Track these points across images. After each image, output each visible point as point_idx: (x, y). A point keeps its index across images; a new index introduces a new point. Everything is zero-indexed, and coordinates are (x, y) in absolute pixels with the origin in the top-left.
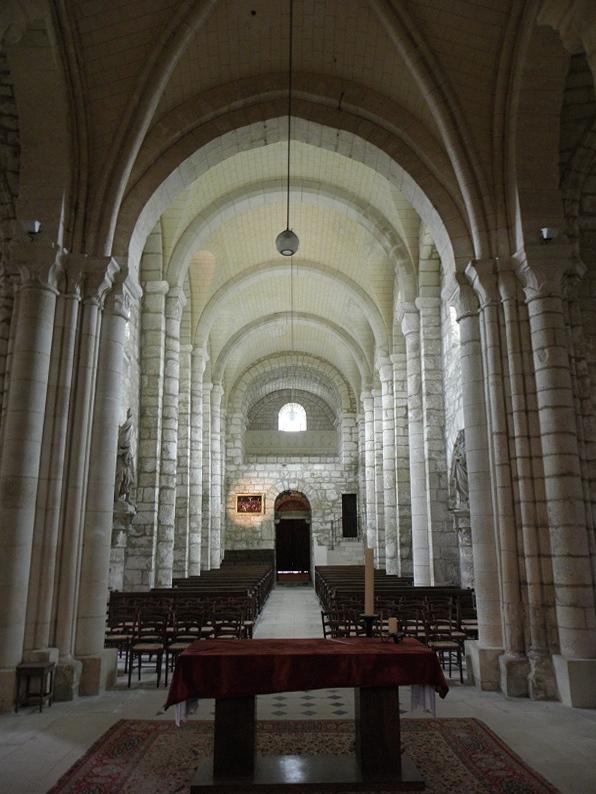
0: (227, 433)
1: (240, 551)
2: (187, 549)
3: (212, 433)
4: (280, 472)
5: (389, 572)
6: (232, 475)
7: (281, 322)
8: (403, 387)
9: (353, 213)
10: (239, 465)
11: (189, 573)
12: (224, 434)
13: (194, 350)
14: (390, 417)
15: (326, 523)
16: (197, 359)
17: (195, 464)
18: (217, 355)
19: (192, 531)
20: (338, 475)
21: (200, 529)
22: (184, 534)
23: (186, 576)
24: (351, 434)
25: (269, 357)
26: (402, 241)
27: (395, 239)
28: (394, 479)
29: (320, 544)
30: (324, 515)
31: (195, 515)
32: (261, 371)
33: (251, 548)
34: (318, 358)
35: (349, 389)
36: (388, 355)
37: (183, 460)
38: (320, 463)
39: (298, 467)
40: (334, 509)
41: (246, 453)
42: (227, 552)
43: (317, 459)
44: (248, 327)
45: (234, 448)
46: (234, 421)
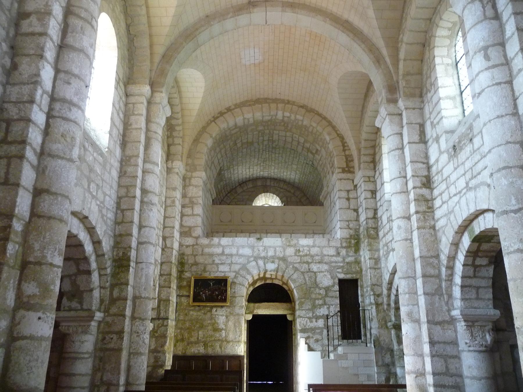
3: (145, 162)
4: (252, 247)
6: (188, 251)
10: (197, 238)
15: (317, 318)
20: (332, 252)
24: (348, 199)
30: (314, 307)
34: (302, 107)
40: (327, 299)
45: (193, 215)
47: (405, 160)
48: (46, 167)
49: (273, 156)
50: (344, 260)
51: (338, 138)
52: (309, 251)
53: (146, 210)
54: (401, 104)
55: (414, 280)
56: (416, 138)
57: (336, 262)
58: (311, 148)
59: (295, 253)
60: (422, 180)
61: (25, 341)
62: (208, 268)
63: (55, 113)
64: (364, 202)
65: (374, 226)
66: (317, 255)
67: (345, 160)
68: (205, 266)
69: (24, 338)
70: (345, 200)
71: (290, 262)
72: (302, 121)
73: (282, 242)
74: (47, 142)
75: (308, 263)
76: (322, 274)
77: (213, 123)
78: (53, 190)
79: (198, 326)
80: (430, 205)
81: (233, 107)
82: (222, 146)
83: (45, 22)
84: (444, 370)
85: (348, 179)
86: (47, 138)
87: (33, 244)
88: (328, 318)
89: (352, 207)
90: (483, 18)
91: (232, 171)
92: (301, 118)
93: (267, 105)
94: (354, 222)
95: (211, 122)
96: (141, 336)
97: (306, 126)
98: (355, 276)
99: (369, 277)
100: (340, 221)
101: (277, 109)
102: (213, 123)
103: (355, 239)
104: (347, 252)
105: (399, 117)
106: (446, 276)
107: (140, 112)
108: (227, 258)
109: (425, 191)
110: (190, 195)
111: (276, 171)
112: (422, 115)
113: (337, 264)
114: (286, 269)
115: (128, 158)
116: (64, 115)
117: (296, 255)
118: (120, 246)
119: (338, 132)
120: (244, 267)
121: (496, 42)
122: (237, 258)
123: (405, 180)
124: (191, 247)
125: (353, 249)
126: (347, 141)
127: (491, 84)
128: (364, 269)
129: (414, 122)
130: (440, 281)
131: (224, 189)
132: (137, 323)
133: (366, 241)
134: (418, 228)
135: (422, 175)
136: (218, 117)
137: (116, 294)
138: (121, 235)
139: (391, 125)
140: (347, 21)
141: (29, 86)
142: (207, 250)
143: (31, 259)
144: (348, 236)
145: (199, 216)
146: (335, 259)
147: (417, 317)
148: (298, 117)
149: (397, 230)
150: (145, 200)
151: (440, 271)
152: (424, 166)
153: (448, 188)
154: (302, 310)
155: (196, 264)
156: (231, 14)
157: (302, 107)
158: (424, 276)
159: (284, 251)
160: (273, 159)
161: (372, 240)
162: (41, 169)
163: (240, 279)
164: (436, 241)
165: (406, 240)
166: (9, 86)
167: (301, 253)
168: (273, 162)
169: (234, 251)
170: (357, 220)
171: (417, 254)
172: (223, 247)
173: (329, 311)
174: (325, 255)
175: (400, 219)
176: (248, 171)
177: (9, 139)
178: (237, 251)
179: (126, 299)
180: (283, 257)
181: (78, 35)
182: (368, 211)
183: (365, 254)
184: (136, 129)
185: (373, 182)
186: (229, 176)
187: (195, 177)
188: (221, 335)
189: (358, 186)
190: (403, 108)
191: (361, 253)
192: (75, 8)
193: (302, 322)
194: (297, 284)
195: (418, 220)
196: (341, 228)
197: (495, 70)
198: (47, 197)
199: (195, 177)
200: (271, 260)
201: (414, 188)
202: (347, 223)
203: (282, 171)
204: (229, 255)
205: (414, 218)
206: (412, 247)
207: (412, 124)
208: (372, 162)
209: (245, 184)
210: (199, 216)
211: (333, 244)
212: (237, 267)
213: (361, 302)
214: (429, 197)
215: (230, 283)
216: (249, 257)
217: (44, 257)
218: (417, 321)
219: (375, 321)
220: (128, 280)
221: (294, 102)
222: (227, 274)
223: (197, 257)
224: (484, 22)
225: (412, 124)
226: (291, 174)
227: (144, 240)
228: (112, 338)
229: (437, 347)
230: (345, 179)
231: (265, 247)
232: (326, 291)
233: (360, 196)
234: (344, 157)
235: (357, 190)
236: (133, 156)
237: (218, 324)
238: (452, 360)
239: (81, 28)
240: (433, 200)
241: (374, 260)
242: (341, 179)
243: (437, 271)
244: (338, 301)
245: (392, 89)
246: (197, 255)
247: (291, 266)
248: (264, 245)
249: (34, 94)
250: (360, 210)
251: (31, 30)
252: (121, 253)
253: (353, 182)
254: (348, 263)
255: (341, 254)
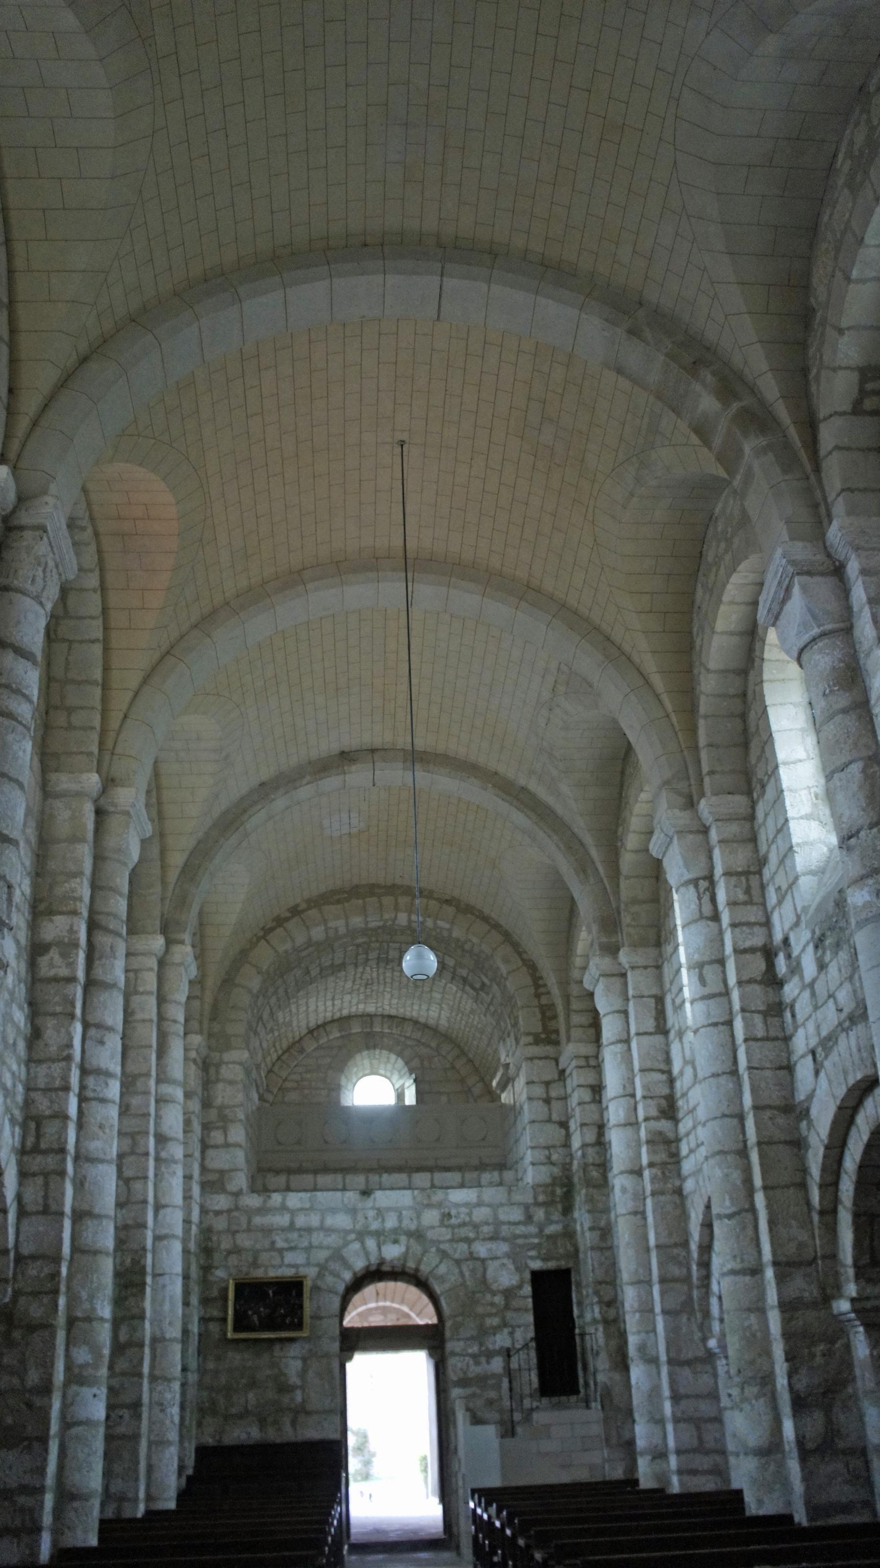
0: (206, 1104)
1: (239, 1449)
2: (54, 1447)
3: (158, 1081)
4: (353, 1211)
5: (755, 1505)
6: (220, 1224)
7: (358, 776)
8: (748, 891)
9: (593, 334)
10: (237, 1194)
11: (56, 1533)
12: (195, 1105)
13: (104, 790)
14: (715, 987)
15: (490, 1355)
16: (114, 823)
17: (94, 1146)
18: (177, 859)
19: (76, 1377)
20: (517, 1215)
21: (104, 1371)
22: (46, 1389)
23: (140, 1514)
24: (547, 1101)
25: (319, 901)
26: (753, 390)
27: (731, 385)
28: (748, 1180)
29: (476, 1421)
30: (484, 1332)
31: (89, 1319)
32: (300, 940)
33: (272, 1435)
34: (448, 902)
35: (537, 981)
36: (690, 804)
37: (50, 1129)
38: (462, 1186)
39: (405, 1198)
40: (509, 1315)
41: (260, 1170)
42: (202, 1452)
43: (456, 1177)
44: (265, 790)
45: (227, 1145)
46: (225, 1072)
47: (632, 1063)
48: (85, 1177)
49: (388, 974)
50: (541, 1231)
51: (525, 969)
52: (470, 1214)
53: (166, 1175)
54: (624, 957)
55: (648, 1287)
56: (650, 1024)
57: (525, 1236)
58: (470, 978)
59: (442, 1221)
60: (659, 1105)
61: (80, 1428)
62: (264, 1257)
63: (90, 1094)
64: (577, 1110)
65: (597, 1161)
66: (487, 1223)
67: (539, 1016)
68: (256, 1254)
69: (79, 1423)
70: (541, 1103)
71: (433, 1242)
72: (450, 931)
73: (414, 1198)
74: (82, 1139)
75: (468, 1241)
76: (497, 1263)
77: (263, 942)
78: (96, 1211)
79: (244, 1381)
80: (673, 1150)
81: (303, 906)
82: (280, 981)
83: (71, 960)
84: (695, 1443)
85: (546, 1058)
86: (82, 1133)
87: (79, 1292)
88: (509, 1356)
89: (555, 1117)
90: (697, 916)
91: (294, 1010)
92: (447, 926)
93: (375, 899)
94: (560, 1150)
95: (259, 939)
96: (169, 1410)
97: (458, 940)
98: (563, 1263)
99: (591, 1268)
100: (532, 1148)
101: (397, 908)
102: (263, 942)
103: (563, 1186)
104: (547, 1213)
105: (622, 980)
106: (698, 1279)
107: (148, 988)
108: (300, 1236)
109: (664, 1125)
110: (219, 1101)
111: (394, 1001)
112: (659, 979)
113: (527, 1241)
114: (423, 1255)
115: (130, 1079)
116: (101, 1095)
117: (442, 1224)
118: (125, 1247)
119: (525, 956)
120: (337, 1255)
121: (713, 957)
122: (322, 1234)
123: (632, 1101)
124: (225, 1214)
125: (560, 1207)
126: (544, 974)
127: (706, 1024)
128: (582, 1248)
129: (646, 993)
130: (690, 1288)
131: (274, 1046)
132: (159, 1388)
133: (584, 1191)
134: (653, 1194)
135: (658, 1094)
136: (272, 929)
137: (123, 1337)
138: (126, 1227)
139: (607, 996)
140: (523, 789)
141: (60, 1065)
142: (258, 1220)
143: (79, 1314)
144: (548, 1180)
145: (240, 1146)
146: (521, 1230)
147: (654, 1353)
148: (440, 923)
149: (620, 1194)
150: (163, 1155)
151: (689, 1270)
152: (664, 1077)
153: (694, 1127)
154: (459, 1340)
155: (236, 1250)
156: (308, 778)
157: (448, 902)
158: (663, 1281)
159: (419, 1217)
160: (388, 980)
161: (595, 1191)
162: (78, 1181)
163: (329, 1279)
164: (684, 1216)
165: (635, 1213)
166: (33, 1065)
167: (453, 1221)
168: (388, 985)
169: (314, 1220)
170: (567, 1145)
171: (652, 1241)
172: (293, 1213)
173: (513, 1339)
174: (503, 1223)
175: (625, 1175)
176: (329, 1003)
177: (43, 1146)
178: (322, 1222)
179: (141, 1345)
180: (417, 1230)
181: (108, 962)
182: (585, 1129)
183: (582, 1218)
184: (144, 1021)
185: (594, 1067)
186: (287, 1019)
187: (227, 1063)
188: (292, 1399)
189: (568, 1072)
190: (627, 966)
191: (576, 1214)
192: (101, 917)
193: (459, 1365)
194: (447, 1286)
195: (653, 1180)
196: (533, 1164)
197: (711, 1002)
198: (89, 1222)
199: (227, 1063)
200: (393, 1237)
201: (646, 1119)
202: (547, 1152)
203: (409, 1002)
204: (305, 1230)
205: (647, 1173)
206: (645, 1226)
207: (643, 997)
208: (590, 1026)
209: (321, 1029)
210: (240, 1146)
211: (517, 1198)
212: (322, 1255)
213: (579, 1317)
214: (671, 1135)
215: (309, 1289)
216: (347, 1232)
217: (93, 1309)
218: (653, 1361)
219: (603, 1356)
220: (143, 1311)
221: (431, 892)
222: (303, 1271)
223: (238, 1236)
224: (699, 923)
225: (643, 997)
226: (428, 1010)
227: (164, 1231)
228: (121, 1417)
229: (683, 1403)
230: (540, 1058)
231: (379, 1210)
232: (507, 1298)
233: (570, 1096)
234: (537, 1010)
235: (564, 1081)
236: (141, 1075)
237: (285, 1375)
238: (709, 1426)
239: (111, 947)
240: (678, 1140)
241: (599, 1232)
242: (531, 1059)
243: (685, 1270)
244: (530, 1318)
245: (610, 923)
246: (237, 1232)
247: (433, 1249)
248: (377, 1206)
249: (69, 1076)
250: (573, 1125)
251: (52, 973)
252: (129, 1260)
253: (557, 1064)
254: (549, 1237)
255: (535, 1219)
